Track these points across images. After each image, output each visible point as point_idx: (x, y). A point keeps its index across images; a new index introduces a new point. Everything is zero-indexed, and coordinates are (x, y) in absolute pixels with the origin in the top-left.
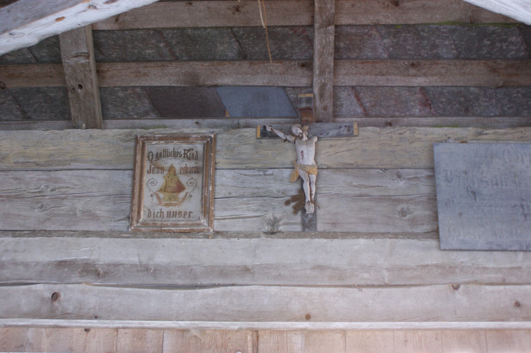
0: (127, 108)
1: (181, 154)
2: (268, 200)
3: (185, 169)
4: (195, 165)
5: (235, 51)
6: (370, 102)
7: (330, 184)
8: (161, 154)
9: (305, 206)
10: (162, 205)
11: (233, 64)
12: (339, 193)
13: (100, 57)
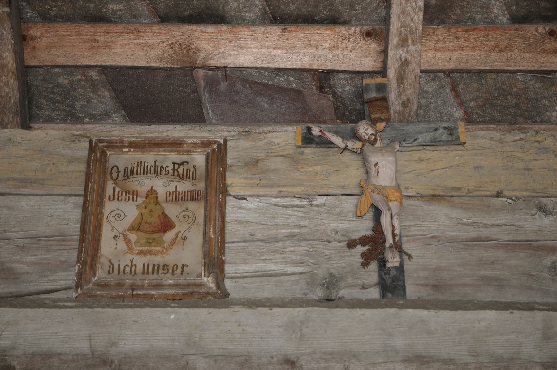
0: (72, 106)
1: (168, 170)
2: (318, 246)
3: (174, 193)
4: (192, 188)
5: (257, 10)
6: (476, 100)
7: (422, 221)
8: (132, 169)
9: (385, 255)
10: (133, 254)
11: (253, 31)
12: (441, 234)
13: (29, 14)
